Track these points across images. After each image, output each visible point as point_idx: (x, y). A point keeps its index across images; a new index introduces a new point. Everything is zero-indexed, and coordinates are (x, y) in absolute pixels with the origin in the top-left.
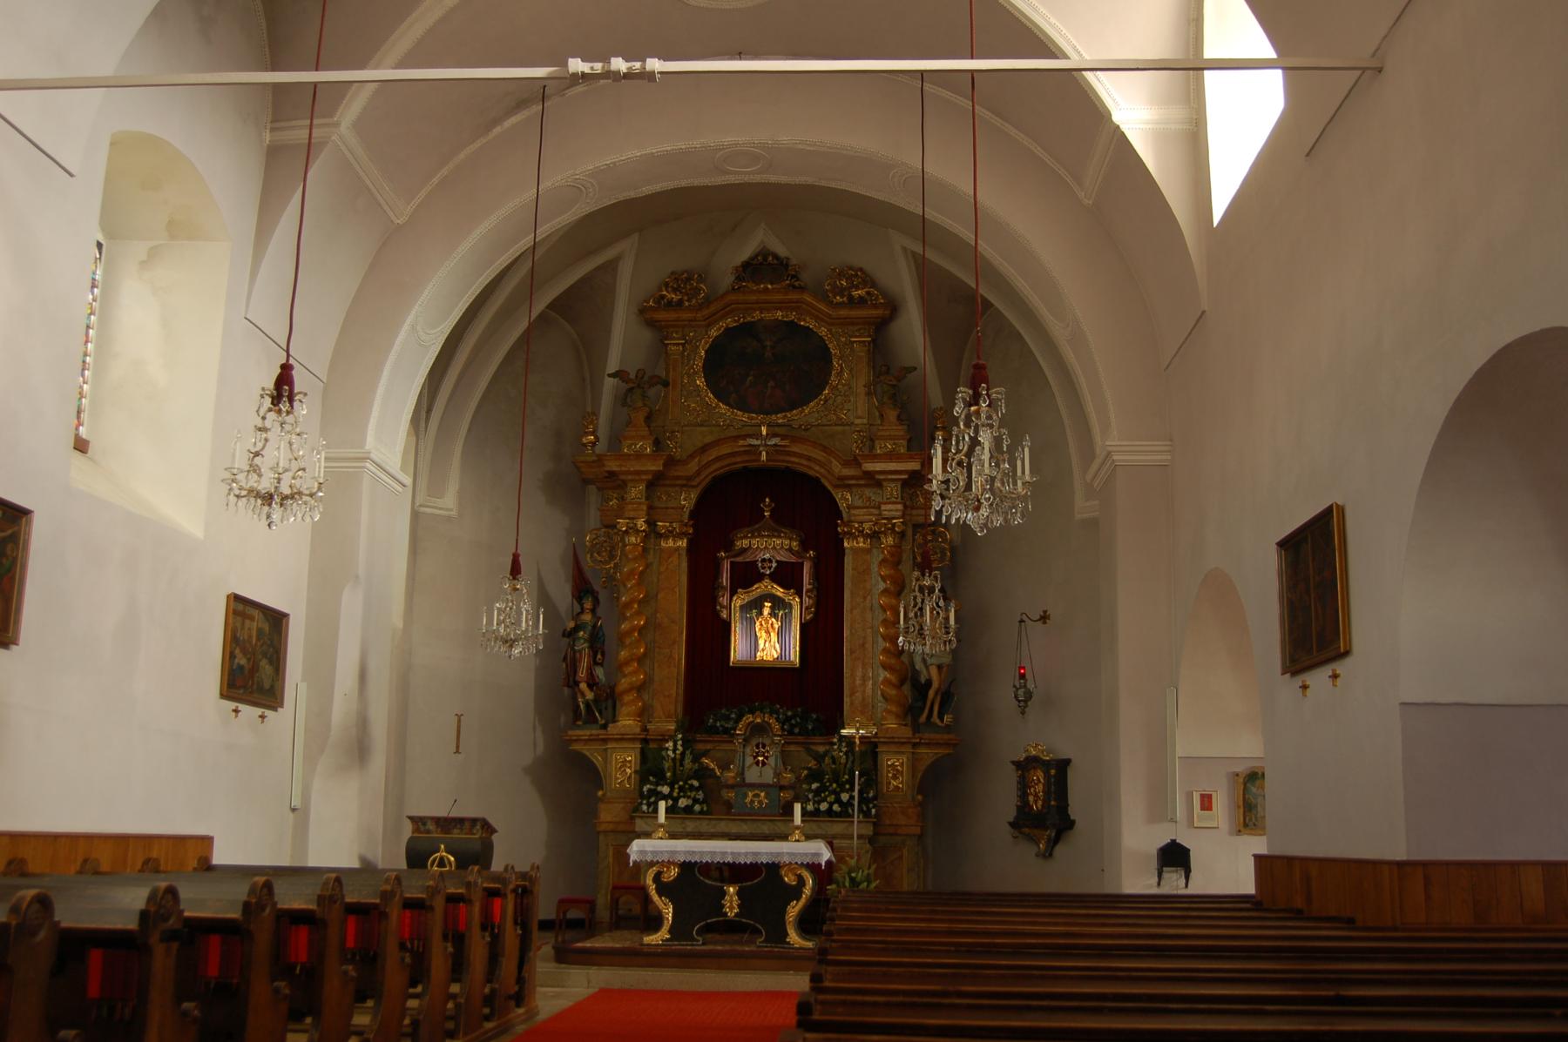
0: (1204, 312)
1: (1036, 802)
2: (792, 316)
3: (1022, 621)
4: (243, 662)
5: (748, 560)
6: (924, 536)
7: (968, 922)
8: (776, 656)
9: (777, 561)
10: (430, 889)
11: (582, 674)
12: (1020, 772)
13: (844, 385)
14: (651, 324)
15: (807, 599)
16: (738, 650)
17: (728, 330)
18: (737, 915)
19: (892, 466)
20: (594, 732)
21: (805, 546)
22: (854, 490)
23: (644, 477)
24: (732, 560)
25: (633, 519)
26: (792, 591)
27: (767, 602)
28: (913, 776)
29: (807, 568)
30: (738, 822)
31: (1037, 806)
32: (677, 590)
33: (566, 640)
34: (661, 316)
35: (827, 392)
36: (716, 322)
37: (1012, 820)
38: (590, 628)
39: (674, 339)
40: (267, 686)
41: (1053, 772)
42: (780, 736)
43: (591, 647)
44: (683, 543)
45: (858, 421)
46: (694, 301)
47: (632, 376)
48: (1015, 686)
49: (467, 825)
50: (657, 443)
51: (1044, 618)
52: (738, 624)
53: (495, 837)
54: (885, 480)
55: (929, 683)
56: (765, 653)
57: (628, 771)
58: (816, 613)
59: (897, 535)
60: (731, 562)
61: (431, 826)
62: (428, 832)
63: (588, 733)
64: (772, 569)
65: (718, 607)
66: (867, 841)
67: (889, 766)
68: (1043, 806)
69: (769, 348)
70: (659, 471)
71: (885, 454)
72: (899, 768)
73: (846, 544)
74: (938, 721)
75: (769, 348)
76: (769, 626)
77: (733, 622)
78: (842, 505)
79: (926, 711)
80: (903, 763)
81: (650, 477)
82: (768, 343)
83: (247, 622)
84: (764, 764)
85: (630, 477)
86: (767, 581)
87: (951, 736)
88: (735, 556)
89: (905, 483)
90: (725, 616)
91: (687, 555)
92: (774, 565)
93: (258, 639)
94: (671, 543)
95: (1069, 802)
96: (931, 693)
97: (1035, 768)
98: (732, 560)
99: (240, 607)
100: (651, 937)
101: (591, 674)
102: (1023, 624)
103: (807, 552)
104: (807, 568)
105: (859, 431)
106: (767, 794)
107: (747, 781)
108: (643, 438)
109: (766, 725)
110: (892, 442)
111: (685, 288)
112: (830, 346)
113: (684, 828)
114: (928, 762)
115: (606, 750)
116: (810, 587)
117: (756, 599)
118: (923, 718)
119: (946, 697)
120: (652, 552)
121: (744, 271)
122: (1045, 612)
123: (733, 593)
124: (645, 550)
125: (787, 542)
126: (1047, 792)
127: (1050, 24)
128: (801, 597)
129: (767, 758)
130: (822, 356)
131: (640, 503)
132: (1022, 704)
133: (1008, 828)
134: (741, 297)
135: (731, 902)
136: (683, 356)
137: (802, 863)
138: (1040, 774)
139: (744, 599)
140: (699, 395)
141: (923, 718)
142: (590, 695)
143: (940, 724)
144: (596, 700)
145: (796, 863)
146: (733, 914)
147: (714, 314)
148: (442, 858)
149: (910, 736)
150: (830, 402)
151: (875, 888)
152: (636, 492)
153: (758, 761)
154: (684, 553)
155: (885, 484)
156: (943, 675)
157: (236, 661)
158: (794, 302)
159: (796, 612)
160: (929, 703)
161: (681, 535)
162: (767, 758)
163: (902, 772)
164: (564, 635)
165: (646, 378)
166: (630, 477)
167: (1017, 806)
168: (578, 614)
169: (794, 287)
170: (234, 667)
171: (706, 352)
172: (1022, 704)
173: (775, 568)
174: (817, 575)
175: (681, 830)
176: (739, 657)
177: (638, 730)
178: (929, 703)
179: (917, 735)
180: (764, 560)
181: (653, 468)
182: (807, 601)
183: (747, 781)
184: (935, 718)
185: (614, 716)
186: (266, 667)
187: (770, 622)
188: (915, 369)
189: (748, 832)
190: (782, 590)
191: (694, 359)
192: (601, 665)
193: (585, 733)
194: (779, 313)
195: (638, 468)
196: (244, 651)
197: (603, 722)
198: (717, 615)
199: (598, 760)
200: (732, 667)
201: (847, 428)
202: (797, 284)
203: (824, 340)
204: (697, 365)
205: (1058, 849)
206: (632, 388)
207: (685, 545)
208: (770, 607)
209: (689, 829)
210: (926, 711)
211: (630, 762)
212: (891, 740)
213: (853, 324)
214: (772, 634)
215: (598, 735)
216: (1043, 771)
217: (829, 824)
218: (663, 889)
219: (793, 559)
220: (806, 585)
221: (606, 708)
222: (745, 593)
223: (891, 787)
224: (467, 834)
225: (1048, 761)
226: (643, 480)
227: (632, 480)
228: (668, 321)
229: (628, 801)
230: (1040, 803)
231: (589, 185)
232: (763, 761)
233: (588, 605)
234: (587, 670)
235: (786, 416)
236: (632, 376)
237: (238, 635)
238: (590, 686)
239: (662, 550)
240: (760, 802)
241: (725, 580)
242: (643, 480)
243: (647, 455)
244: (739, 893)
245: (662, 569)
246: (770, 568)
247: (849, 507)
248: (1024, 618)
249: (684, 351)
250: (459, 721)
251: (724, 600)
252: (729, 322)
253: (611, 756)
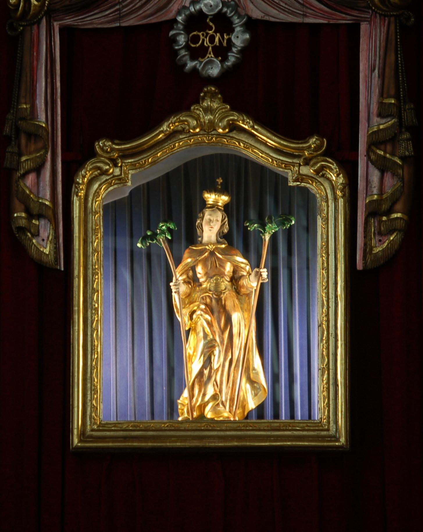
7: (289, 10)
8: (252, 405)
15: (375, 175)
24: (69, 21)
26: (313, 141)
27: (213, 189)
52: (98, 282)
56: (210, 391)
60: (63, 30)
64: (232, 59)
65: (20, 215)
76: (225, 283)
77: (78, 270)
98: (69, 21)
116: (384, 124)
117: (168, 176)
139: (121, 180)
151: (341, 192)
171: (369, 202)
173: (242, 51)
187: (228, 268)
200: (80, 452)
208: (227, 208)
214: (236, 317)
222: (125, 155)
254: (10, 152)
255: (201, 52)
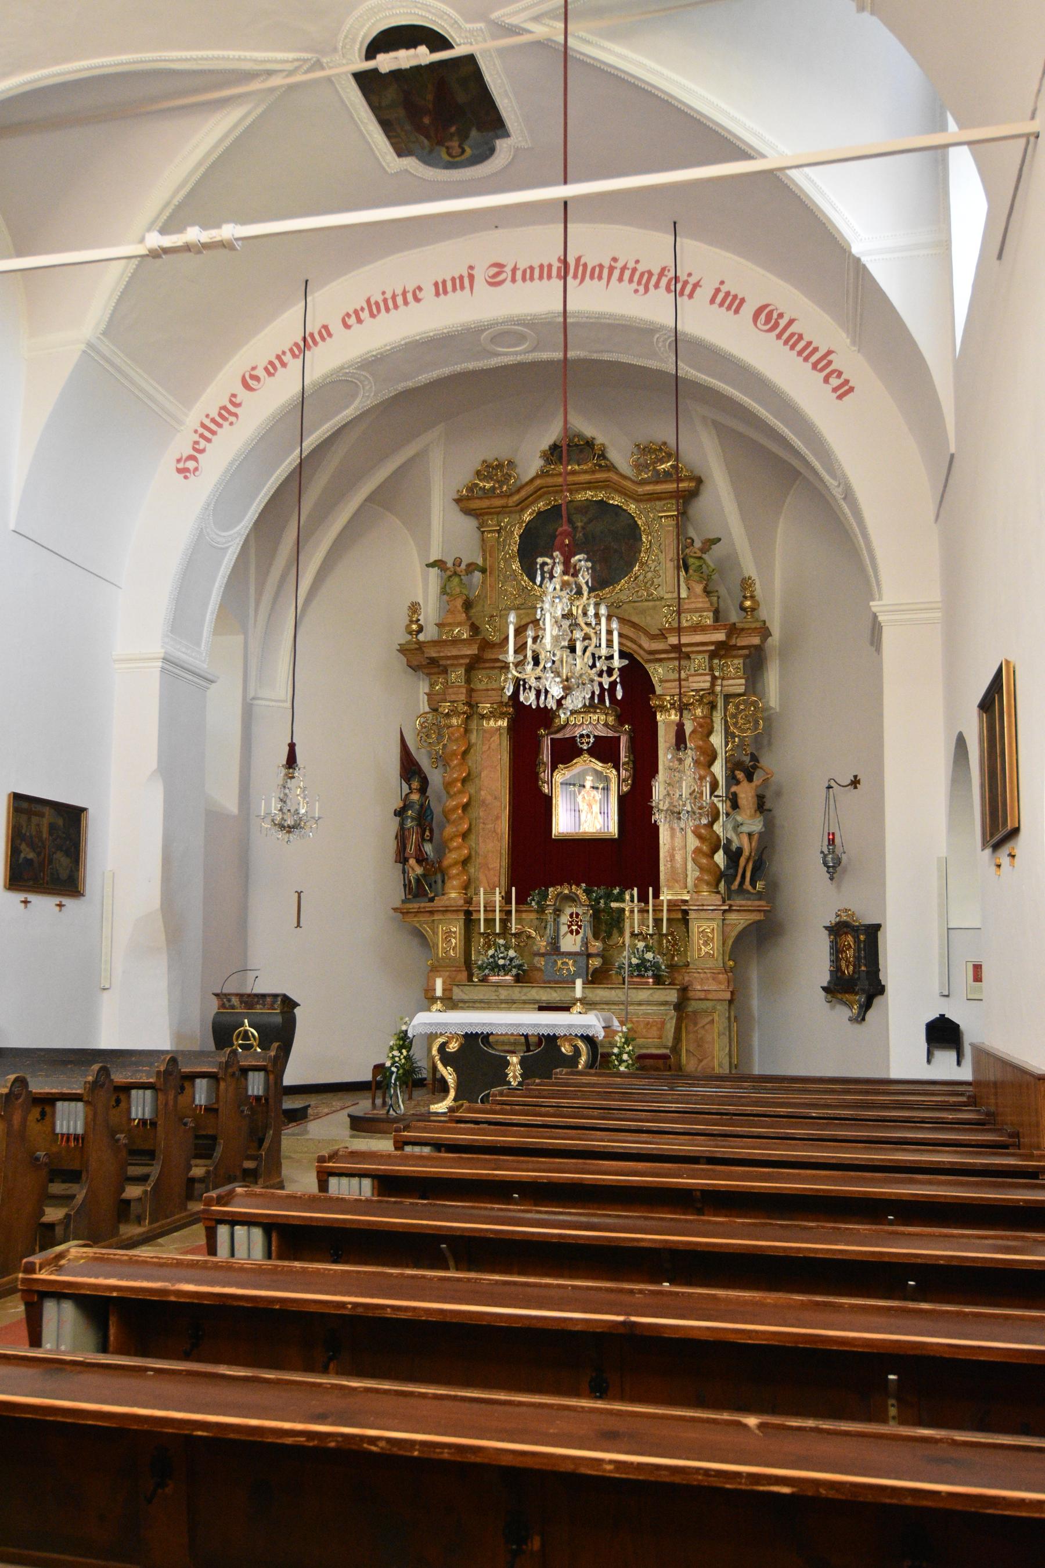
0: (952, 456)
1: (847, 967)
2: (601, 495)
3: (829, 787)
4: (31, 855)
5: (567, 736)
6: (737, 706)
8: (598, 828)
9: (595, 736)
10: (88, 1086)
11: (411, 850)
12: (832, 937)
13: (653, 561)
14: (468, 512)
16: (563, 824)
17: (539, 513)
18: (520, 1084)
19: (698, 638)
20: (422, 905)
21: (621, 720)
22: (665, 664)
23: (462, 661)
25: (454, 702)
28: (723, 944)
29: (624, 741)
30: (548, 989)
31: (849, 971)
32: (498, 768)
33: (398, 819)
34: (476, 504)
35: (637, 568)
36: (528, 507)
37: (825, 984)
38: (418, 807)
39: (489, 526)
40: (64, 875)
41: (862, 937)
42: (588, 906)
43: (419, 825)
44: (503, 723)
45: (667, 596)
46: (505, 488)
47: (450, 565)
48: (822, 852)
49: (269, 999)
50: (475, 629)
51: (855, 782)
53: (297, 1011)
54: (693, 652)
55: (740, 851)
57: (453, 941)
58: (633, 785)
59: (706, 707)
60: (551, 739)
61: (235, 1001)
62: (233, 1007)
63: (416, 905)
66: (672, 1007)
67: (699, 933)
68: (854, 971)
69: (580, 529)
70: (475, 655)
71: (689, 627)
72: (709, 934)
73: (658, 717)
74: (750, 888)
75: (580, 529)
78: (655, 680)
79: (739, 879)
80: (713, 929)
81: (468, 661)
82: (579, 524)
83: (35, 820)
84: (578, 933)
85: (449, 662)
86: (586, 756)
87: (762, 903)
88: (557, 732)
89: (713, 655)
90: (547, 791)
91: (508, 733)
92: (592, 740)
93: (50, 834)
94: (492, 723)
95: (880, 967)
96: (742, 861)
97: (846, 933)
99: (25, 805)
100: (436, 1106)
101: (419, 849)
102: (831, 790)
103: (622, 725)
104: (624, 741)
105: (669, 606)
106: (575, 961)
107: (562, 950)
108: (459, 624)
109: (574, 896)
110: (698, 614)
111: (496, 475)
112: (639, 522)
113: (498, 996)
114: (740, 928)
115: (433, 920)
118: (735, 885)
119: (759, 867)
120: (475, 732)
121: (552, 454)
122: (855, 777)
123: (554, 768)
124: (467, 731)
125: (603, 717)
126: (857, 958)
127: (172, 61)
128: (618, 771)
129: (580, 927)
130: (632, 533)
131: (460, 687)
132: (831, 870)
133: (823, 993)
134: (550, 481)
135: (514, 1072)
136: (499, 542)
137: (582, 1035)
138: (850, 938)
140: (515, 580)
141: (735, 885)
142: (419, 870)
143: (752, 890)
144: (424, 876)
145: (576, 1035)
146: (517, 1083)
147: (526, 499)
148: (246, 1032)
149: (720, 903)
150: (641, 578)
152: (457, 675)
153: (572, 930)
154: (505, 732)
155: (693, 656)
156: (753, 844)
157: (22, 855)
158: (601, 482)
159: (614, 787)
160: (740, 871)
161: (502, 715)
162: (580, 927)
163: (713, 938)
164: (395, 815)
165: (463, 566)
166: (449, 662)
167: (831, 971)
168: (407, 795)
169: (600, 466)
170: (21, 861)
171: (520, 536)
172: (831, 870)
174: (633, 748)
175: (496, 998)
176: (561, 831)
177: (462, 902)
178: (740, 871)
179: (728, 902)
180: (582, 736)
181: (469, 652)
182: (624, 774)
183: (562, 950)
184: (747, 885)
185: (443, 889)
186: (62, 860)
188: (719, 540)
189: (558, 999)
190: (601, 764)
191: (510, 545)
192: (431, 840)
193: (414, 906)
194: (589, 493)
195: (454, 653)
196: (32, 846)
197: (433, 895)
198: (539, 790)
199: (427, 930)
201: (658, 603)
202: (603, 463)
203: (633, 517)
204: (512, 550)
205: (870, 1015)
206: (450, 577)
207: (505, 724)
209: (502, 997)
210: (739, 879)
211: (455, 933)
212: (701, 908)
213: (660, 499)
215: (424, 908)
216: (853, 937)
217: (634, 991)
218: (447, 1058)
219: (611, 734)
220: (623, 759)
221: (435, 882)
222: (565, 768)
223: (703, 953)
224: (269, 1009)
225: (857, 926)
226: (461, 665)
227: (452, 665)
228: (481, 509)
229: (454, 969)
230: (851, 968)
231: (362, 378)
232: (577, 930)
233: (415, 785)
234: (415, 847)
235: (598, 595)
236: (450, 565)
237: (23, 831)
238: (419, 862)
239: (485, 731)
240: (568, 970)
241: (546, 756)
242: (461, 665)
243: (464, 640)
244: (522, 1063)
245: (485, 748)
246: (588, 743)
247: (661, 681)
248: (833, 783)
249: (499, 537)
250: (299, 897)
251: (544, 775)
252: (541, 505)
253: (438, 928)
254: (455, 864)
255: (583, 743)
